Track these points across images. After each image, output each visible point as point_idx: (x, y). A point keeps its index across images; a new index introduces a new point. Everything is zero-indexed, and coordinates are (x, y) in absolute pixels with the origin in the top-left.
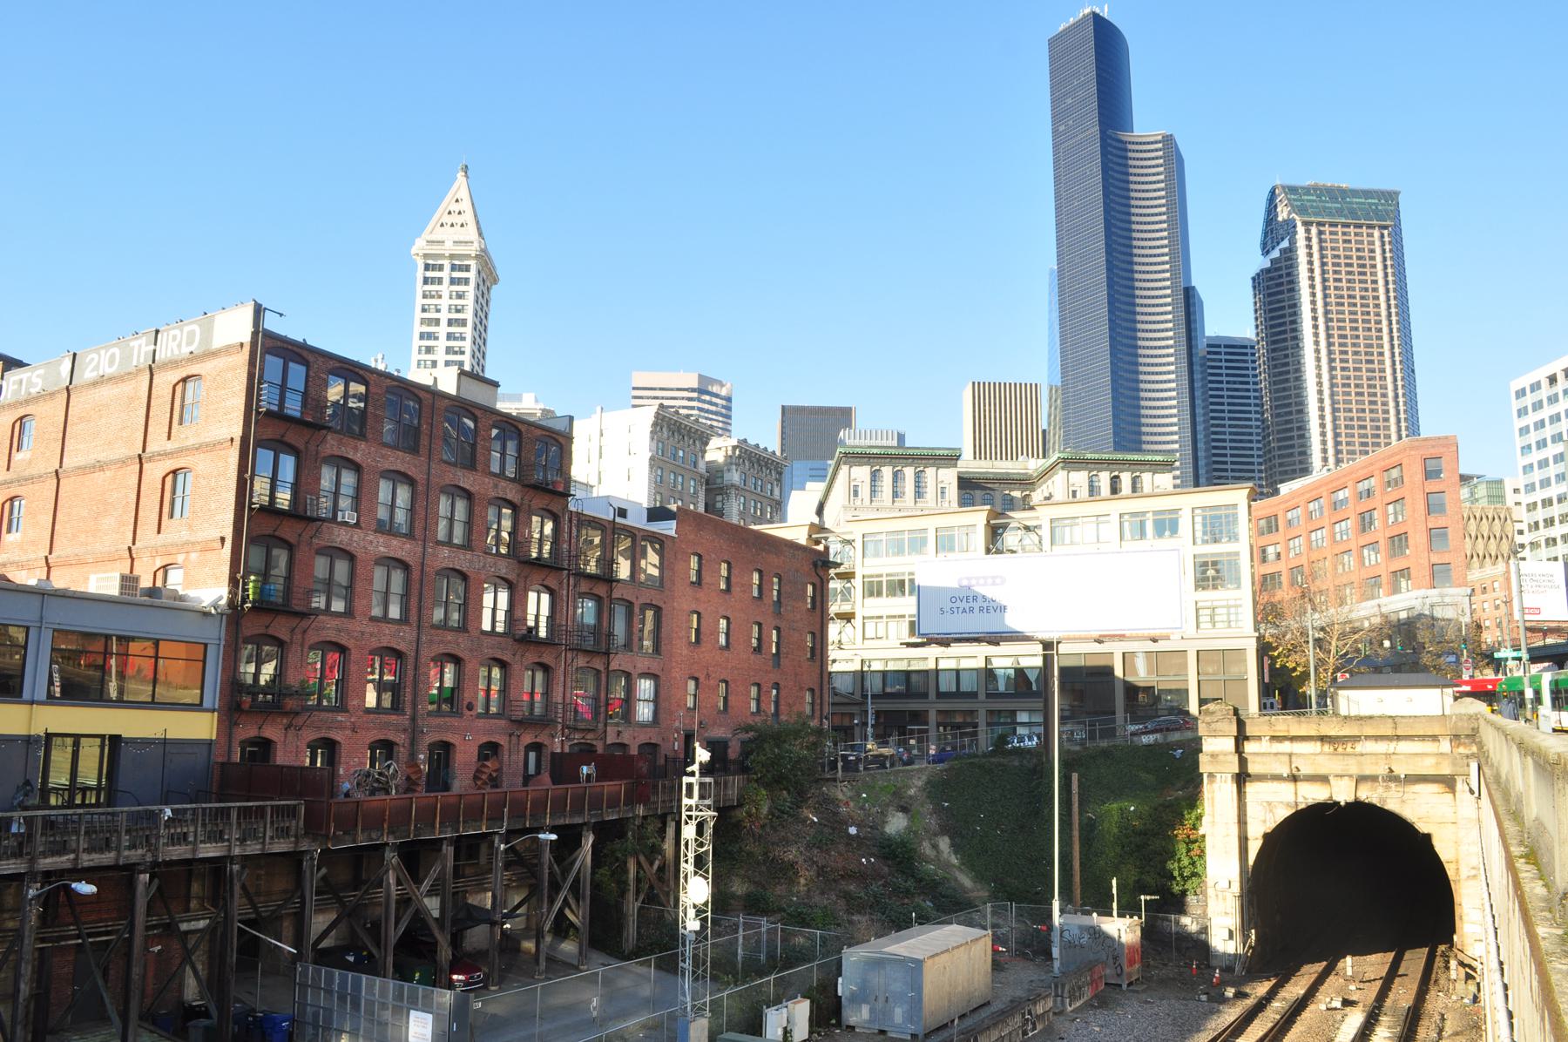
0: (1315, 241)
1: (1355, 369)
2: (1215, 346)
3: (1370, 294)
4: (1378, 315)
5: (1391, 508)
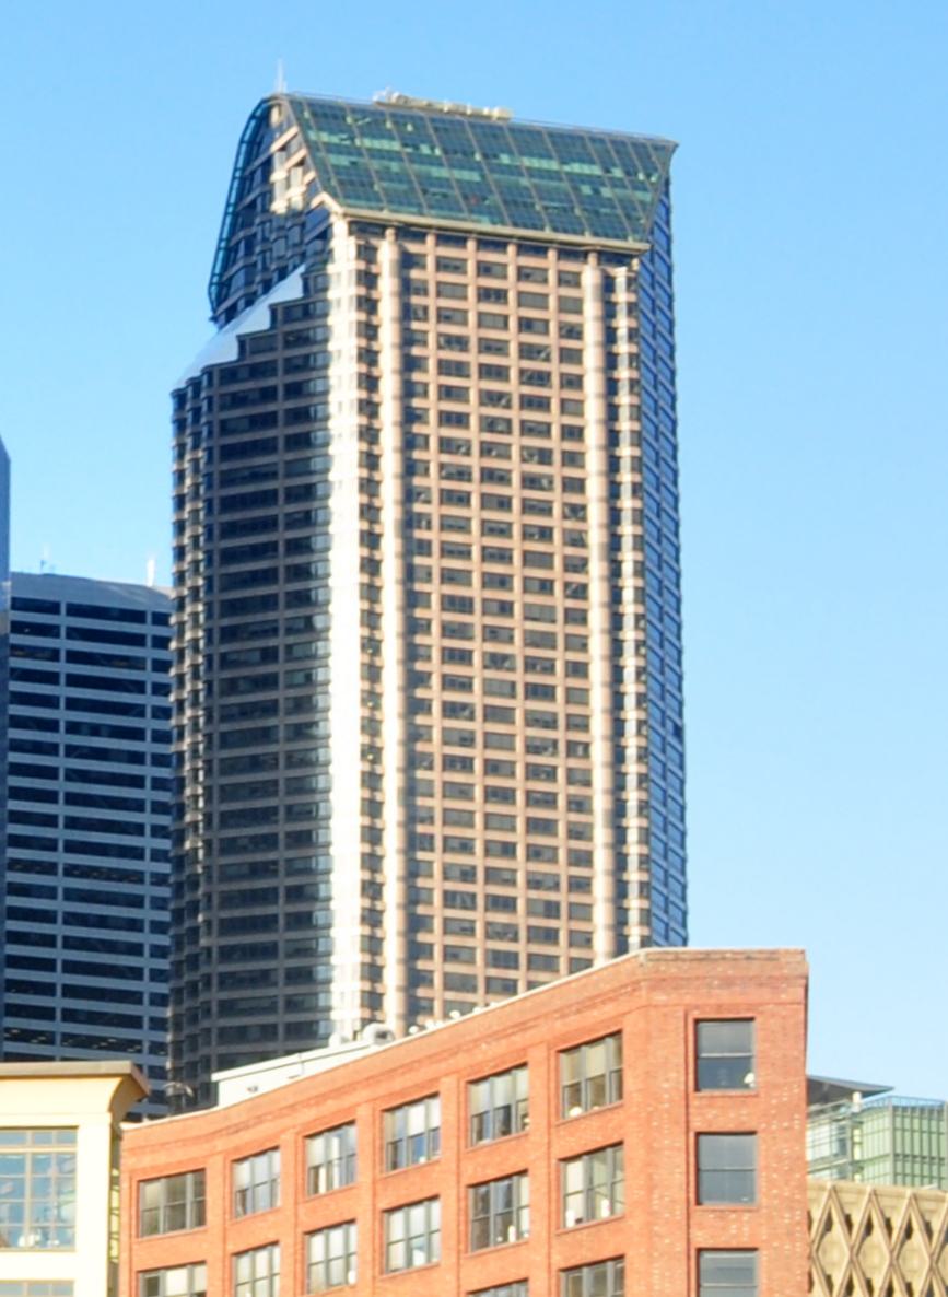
0: (387, 286)
1: (491, 714)
3: (556, 470)
4: (578, 540)
5: (575, 1172)
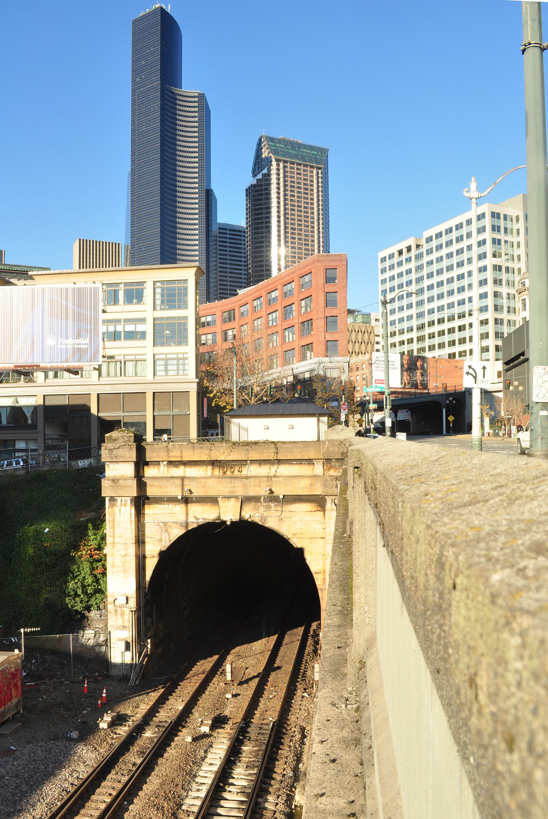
0: (281, 171)
1: (299, 248)
2: (225, 229)
3: (309, 206)
4: (313, 218)
5: (303, 302)
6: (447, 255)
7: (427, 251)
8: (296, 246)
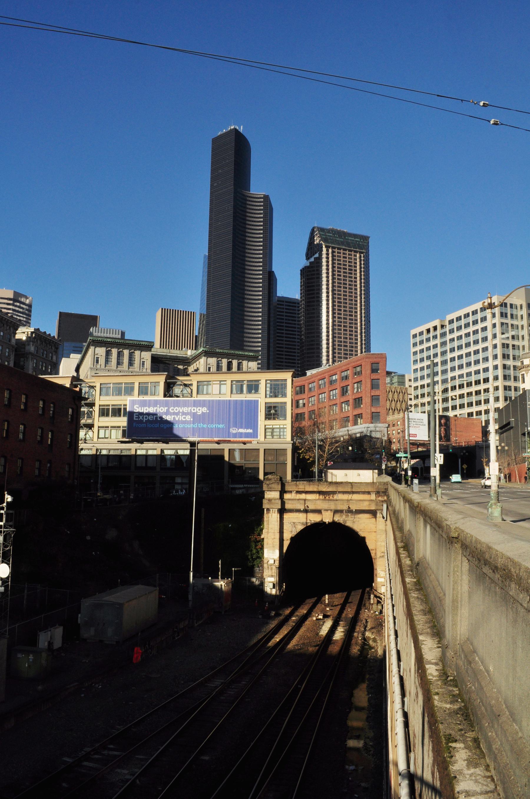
0: (330, 255)
1: (344, 318)
4: (356, 293)
5: (356, 385)
6: (466, 334)
7: (450, 330)
8: (342, 316)
